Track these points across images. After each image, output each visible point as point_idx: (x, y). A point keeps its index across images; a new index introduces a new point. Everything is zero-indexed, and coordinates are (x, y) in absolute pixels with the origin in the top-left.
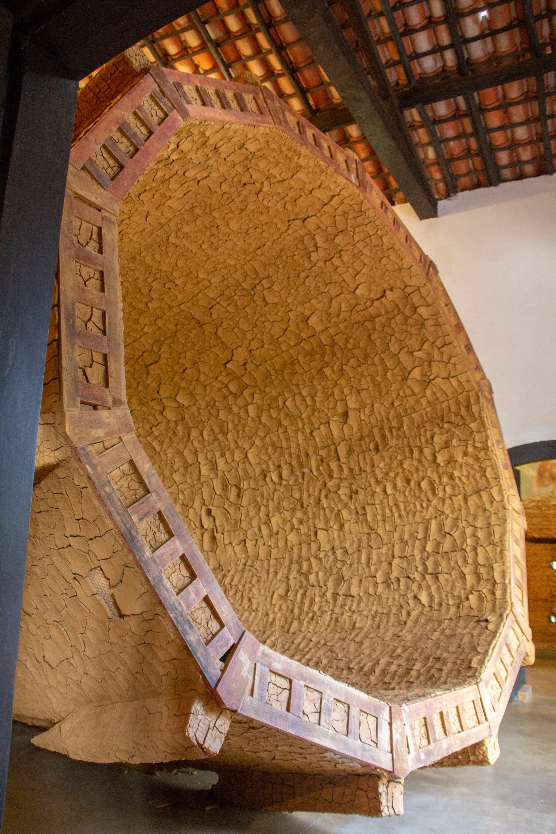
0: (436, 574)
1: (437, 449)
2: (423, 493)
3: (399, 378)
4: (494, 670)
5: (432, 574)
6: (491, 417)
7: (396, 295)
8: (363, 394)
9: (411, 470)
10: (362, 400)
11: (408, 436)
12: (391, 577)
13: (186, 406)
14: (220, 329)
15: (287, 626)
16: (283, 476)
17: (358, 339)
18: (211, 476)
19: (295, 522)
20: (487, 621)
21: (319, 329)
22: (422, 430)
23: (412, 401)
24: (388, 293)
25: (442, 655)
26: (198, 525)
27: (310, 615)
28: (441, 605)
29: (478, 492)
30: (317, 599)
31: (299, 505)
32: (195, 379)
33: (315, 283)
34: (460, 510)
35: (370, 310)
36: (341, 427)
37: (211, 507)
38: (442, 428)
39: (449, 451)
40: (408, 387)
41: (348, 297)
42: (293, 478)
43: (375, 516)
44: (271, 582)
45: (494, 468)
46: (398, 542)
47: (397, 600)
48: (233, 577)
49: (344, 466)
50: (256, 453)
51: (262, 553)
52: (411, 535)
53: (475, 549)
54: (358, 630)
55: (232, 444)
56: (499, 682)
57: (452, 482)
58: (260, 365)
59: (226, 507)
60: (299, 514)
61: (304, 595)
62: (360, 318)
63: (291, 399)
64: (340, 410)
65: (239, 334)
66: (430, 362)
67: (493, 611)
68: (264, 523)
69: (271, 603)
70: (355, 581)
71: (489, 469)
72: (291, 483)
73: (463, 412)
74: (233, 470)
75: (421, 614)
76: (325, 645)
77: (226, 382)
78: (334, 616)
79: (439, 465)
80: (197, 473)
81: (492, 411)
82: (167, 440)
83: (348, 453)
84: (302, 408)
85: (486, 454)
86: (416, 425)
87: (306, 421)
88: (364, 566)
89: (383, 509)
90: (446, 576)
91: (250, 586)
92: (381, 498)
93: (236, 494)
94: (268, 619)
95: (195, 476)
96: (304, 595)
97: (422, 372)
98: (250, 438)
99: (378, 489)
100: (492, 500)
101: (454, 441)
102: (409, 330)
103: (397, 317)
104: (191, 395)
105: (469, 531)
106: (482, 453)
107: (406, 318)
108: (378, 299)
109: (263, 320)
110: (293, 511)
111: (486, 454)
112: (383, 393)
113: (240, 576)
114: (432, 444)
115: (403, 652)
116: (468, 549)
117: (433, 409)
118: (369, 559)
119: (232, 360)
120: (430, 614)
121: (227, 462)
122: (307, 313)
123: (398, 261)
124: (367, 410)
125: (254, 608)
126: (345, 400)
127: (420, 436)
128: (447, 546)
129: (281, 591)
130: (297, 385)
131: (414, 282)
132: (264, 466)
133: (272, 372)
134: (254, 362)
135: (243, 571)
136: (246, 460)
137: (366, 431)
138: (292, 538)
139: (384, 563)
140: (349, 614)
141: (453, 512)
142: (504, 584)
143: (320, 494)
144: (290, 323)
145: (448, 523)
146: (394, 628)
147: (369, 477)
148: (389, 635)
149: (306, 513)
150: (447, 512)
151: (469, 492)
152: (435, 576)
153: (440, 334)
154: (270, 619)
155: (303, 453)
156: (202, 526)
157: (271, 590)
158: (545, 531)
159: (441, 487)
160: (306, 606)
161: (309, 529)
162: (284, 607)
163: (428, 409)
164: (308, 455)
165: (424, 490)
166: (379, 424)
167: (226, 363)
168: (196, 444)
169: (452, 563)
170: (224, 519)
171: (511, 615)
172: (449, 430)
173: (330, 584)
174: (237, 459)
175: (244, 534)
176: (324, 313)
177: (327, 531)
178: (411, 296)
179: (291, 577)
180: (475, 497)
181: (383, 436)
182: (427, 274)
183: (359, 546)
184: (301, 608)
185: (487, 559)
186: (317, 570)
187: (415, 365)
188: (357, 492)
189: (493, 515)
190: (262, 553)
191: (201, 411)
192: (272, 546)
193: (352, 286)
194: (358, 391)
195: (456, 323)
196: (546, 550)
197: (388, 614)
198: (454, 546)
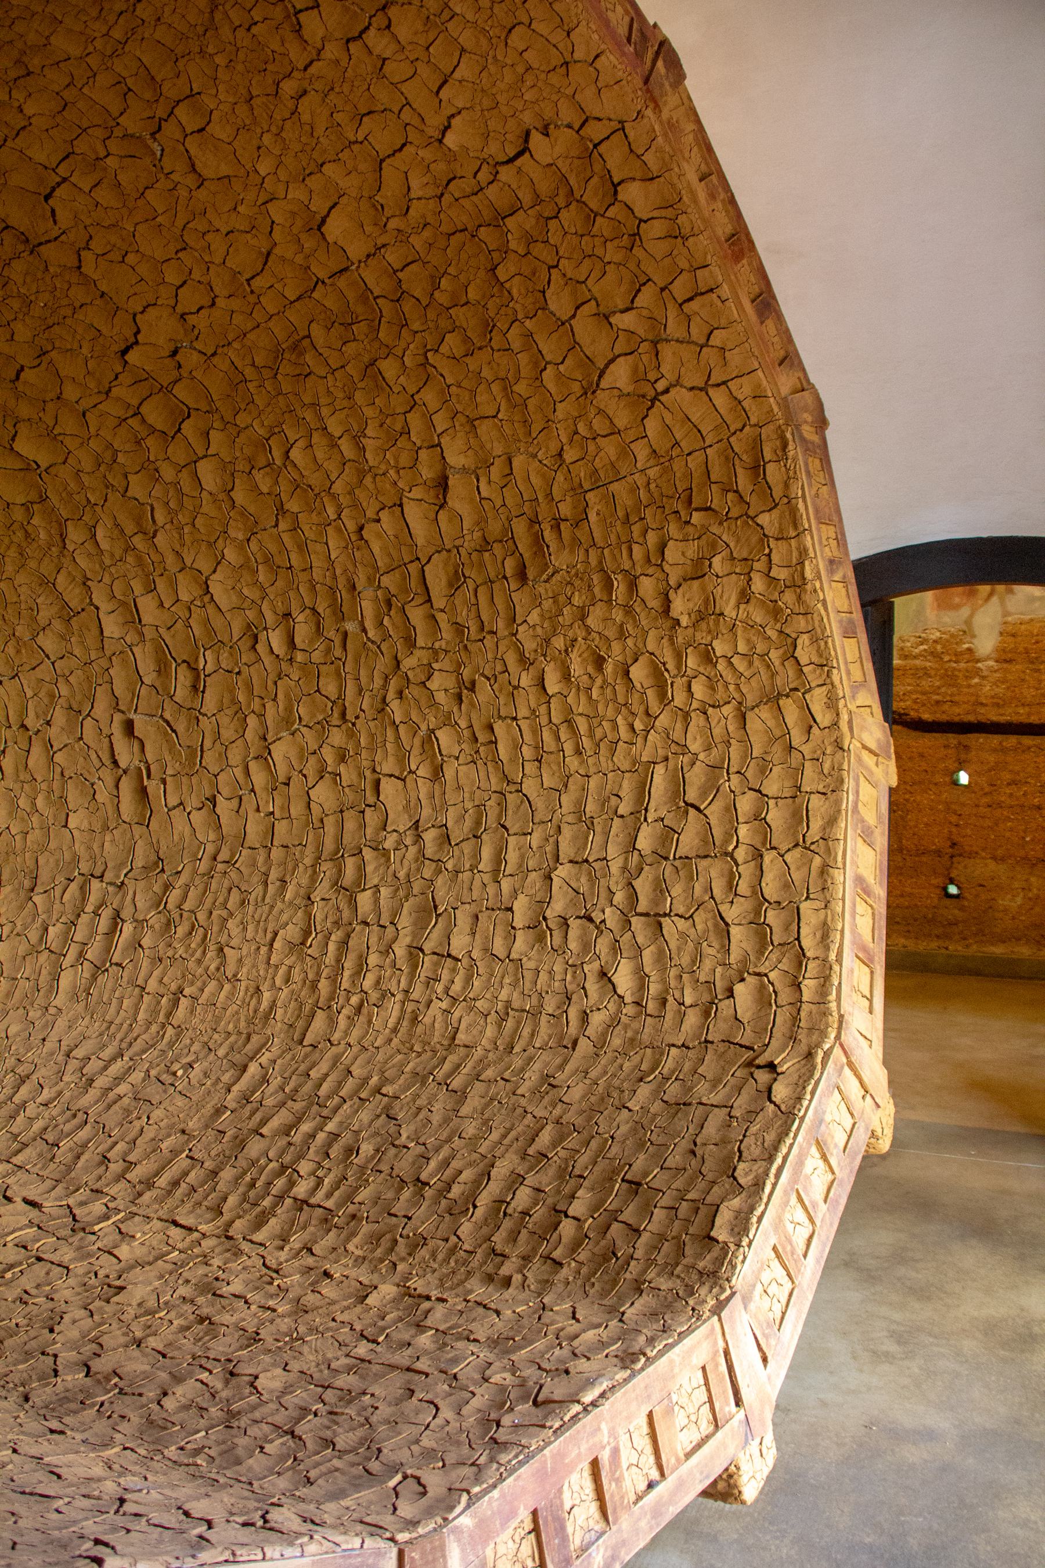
0: (657, 915)
1: (672, 582)
2: (636, 696)
3: (576, 388)
4: (773, 1240)
5: (647, 915)
6: (817, 495)
7: (558, 150)
8: (484, 428)
9: (606, 633)
10: (482, 447)
11: (600, 544)
12: (548, 914)
13: (44, 465)
14: (87, 256)
15: (300, 1024)
16: (298, 640)
17: (462, 278)
18: (128, 639)
19: (328, 755)
20: (771, 1067)
21: (356, 250)
22: (636, 529)
23: (610, 448)
24: (536, 140)
25: (646, 1174)
26: (107, 760)
27: (354, 1000)
28: (664, 1002)
29: (773, 699)
30: (373, 959)
31: (336, 715)
32: (52, 395)
33: (326, 113)
34: (728, 744)
35: (492, 192)
36: (432, 515)
37: (132, 716)
38: (688, 523)
39: (703, 589)
40: (600, 411)
41: (425, 154)
42: (320, 646)
43: (517, 747)
44: (272, 907)
45: (819, 639)
46: (570, 819)
47: (558, 977)
48: (187, 888)
49: (441, 617)
50: (230, 583)
51: (254, 833)
52: (604, 802)
53: (758, 856)
54: (462, 1051)
55: (170, 560)
56: (785, 1268)
57: (708, 670)
58: (214, 354)
59: (167, 715)
60: (337, 737)
61: (344, 943)
62: (464, 218)
63: (301, 444)
64: (427, 472)
65: (143, 270)
66: (655, 343)
67: (793, 1038)
68: (256, 758)
69: (268, 963)
70: (463, 918)
71: (804, 640)
72: (317, 657)
73: (744, 482)
74: (180, 624)
75: (614, 1022)
76: (378, 1091)
77: (135, 402)
78: (410, 1007)
79: (677, 622)
80: (95, 631)
81: (821, 478)
82: (12, 553)
83: (450, 585)
84: (332, 467)
85: (799, 598)
86: (621, 513)
87: (345, 500)
88: (487, 878)
89: (536, 731)
90: (681, 923)
91: (224, 913)
92: (533, 705)
93: (188, 683)
94: (259, 1003)
95: (91, 640)
96: (344, 943)
97: (635, 370)
98: (211, 545)
99: (526, 680)
100: (810, 723)
101: (716, 561)
102: (600, 251)
103: (564, 215)
104: (51, 436)
105: (746, 804)
106: (789, 597)
107: (592, 217)
108: (511, 161)
109: (200, 228)
110: (323, 727)
111: (799, 598)
112: (536, 428)
113: (201, 888)
114: (660, 565)
115: (554, 1145)
116: (741, 854)
117: (665, 471)
118: (499, 859)
119: (137, 343)
120: (635, 1025)
121: (162, 605)
122: (319, 206)
123: (558, 37)
124: (495, 472)
125: (229, 975)
126: (439, 445)
127: (630, 543)
128: (688, 841)
129: (292, 932)
130: (315, 405)
131: (609, 106)
132: (251, 614)
133: (249, 372)
134: (198, 345)
135: (209, 875)
136: (207, 598)
137: (495, 528)
138: (322, 794)
139: (533, 875)
140: (444, 1005)
141: (708, 749)
142: (825, 960)
143: (385, 686)
144: (277, 235)
145: (696, 777)
146: (545, 1056)
147: (502, 648)
148: (532, 1076)
149: (351, 735)
150: (694, 747)
151: (750, 700)
152: (656, 920)
153: (683, 264)
154: (265, 1005)
155: (342, 582)
156: (115, 763)
157: (270, 929)
158: (946, 707)
159: (680, 682)
160: (347, 974)
161: (361, 775)
162: (297, 975)
163: (652, 473)
164: (354, 587)
165: (638, 686)
166: (526, 508)
167: (124, 352)
168: (83, 562)
169: (698, 888)
170: (165, 746)
171: (837, 1051)
172: (706, 529)
173: (405, 921)
174: (185, 596)
175: (210, 782)
176: (364, 205)
177: (404, 780)
178: (602, 148)
179: (316, 896)
180: (765, 712)
181: (538, 542)
182: (646, 81)
183: (478, 823)
184: (334, 980)
185: (787, 885)
186: (376, 881)
187: (616, 352)
188: (472, 688)
189: (807, 764)
190: (254, 831)
191: (85, 479)
192: (277, 815)
193: (435, 121)
194: (471, 423)
195: (729, 229)
196: (946, 747)
197: (535, 1014)
198: (705, 842)
